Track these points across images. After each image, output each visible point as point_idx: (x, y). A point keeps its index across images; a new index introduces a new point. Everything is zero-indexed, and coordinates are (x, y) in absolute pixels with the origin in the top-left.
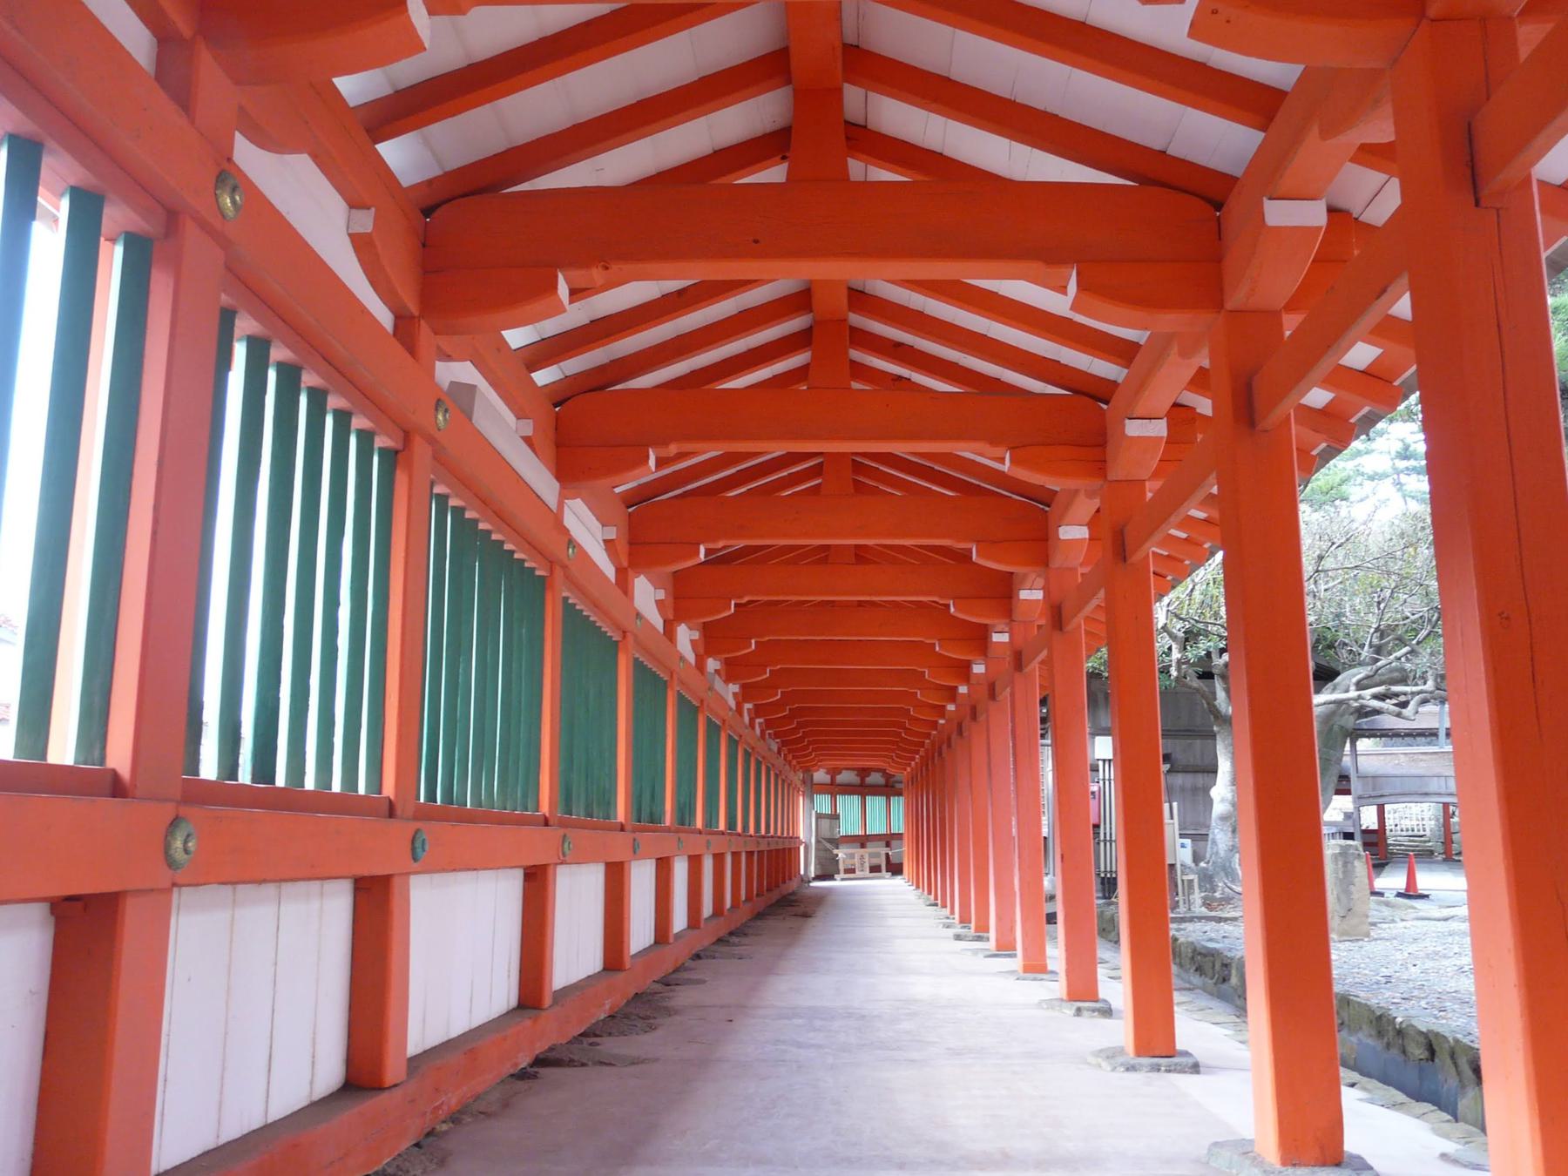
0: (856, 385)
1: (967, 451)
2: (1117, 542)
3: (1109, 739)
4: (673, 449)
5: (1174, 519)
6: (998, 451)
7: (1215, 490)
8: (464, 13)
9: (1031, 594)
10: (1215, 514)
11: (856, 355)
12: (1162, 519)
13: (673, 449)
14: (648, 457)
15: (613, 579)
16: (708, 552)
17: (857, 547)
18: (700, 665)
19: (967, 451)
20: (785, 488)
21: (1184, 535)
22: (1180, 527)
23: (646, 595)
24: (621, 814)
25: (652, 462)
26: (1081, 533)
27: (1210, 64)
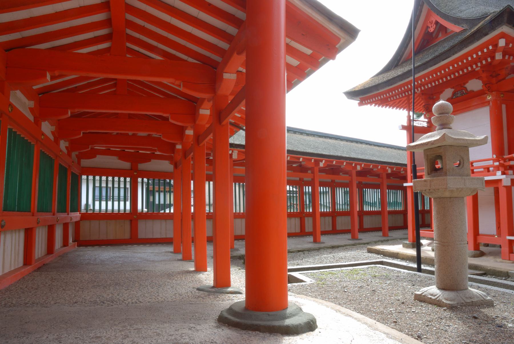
0: (128, 56)
1: (166, 81)
2: (220, 115)
3: (364, 227)
4: (57, 73)
5: (236, 110)
6: (177, 82)
7: (243, 108)
8: (287, 308)
9: (189, 132)
10: (244, 116)
11: (129, 45)
12: (233, 109)
13: (57, 73)
14: (46, 76)
15: (33, 121)
16: (71, 113)
17: (129, 114)
18: (69, 154)
19: (166, 81)
20: (101, 91)
21: (239, 116)
22: (238, 113)
23: (47, 128)
24: (211, 173)
25: (48, 77)
26: (207, 112)
27: (227, 31)
